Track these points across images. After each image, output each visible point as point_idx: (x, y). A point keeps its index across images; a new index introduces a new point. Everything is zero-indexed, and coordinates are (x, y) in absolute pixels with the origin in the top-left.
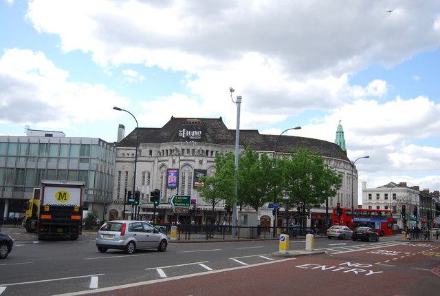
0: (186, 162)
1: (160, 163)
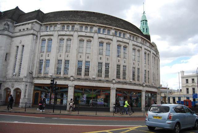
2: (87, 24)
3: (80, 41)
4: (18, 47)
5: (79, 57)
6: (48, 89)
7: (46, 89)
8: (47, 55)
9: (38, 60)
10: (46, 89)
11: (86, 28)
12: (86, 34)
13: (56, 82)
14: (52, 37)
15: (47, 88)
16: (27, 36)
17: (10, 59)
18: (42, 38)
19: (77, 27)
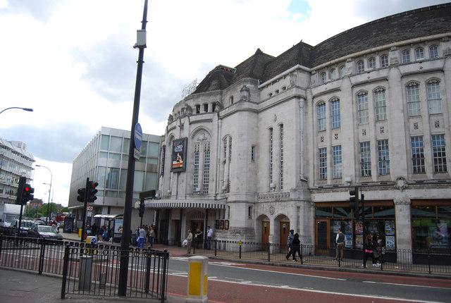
0: (199, 125)
2: (421, 42)
3: (408, 86)
4: (271, 129)
5: (412, 127)
6: (345, 213)
7: (342, 214)
8: (334, 136)
9: (316, 151)
10: (342, 214)
11: (420, 51)
12: (421, 68)
13: (363, 196)
14: (338, 94)
15: (342, 211)
16: (276, 107)
17: (261, 157)
18: (316, 100)
19: (394, 55)
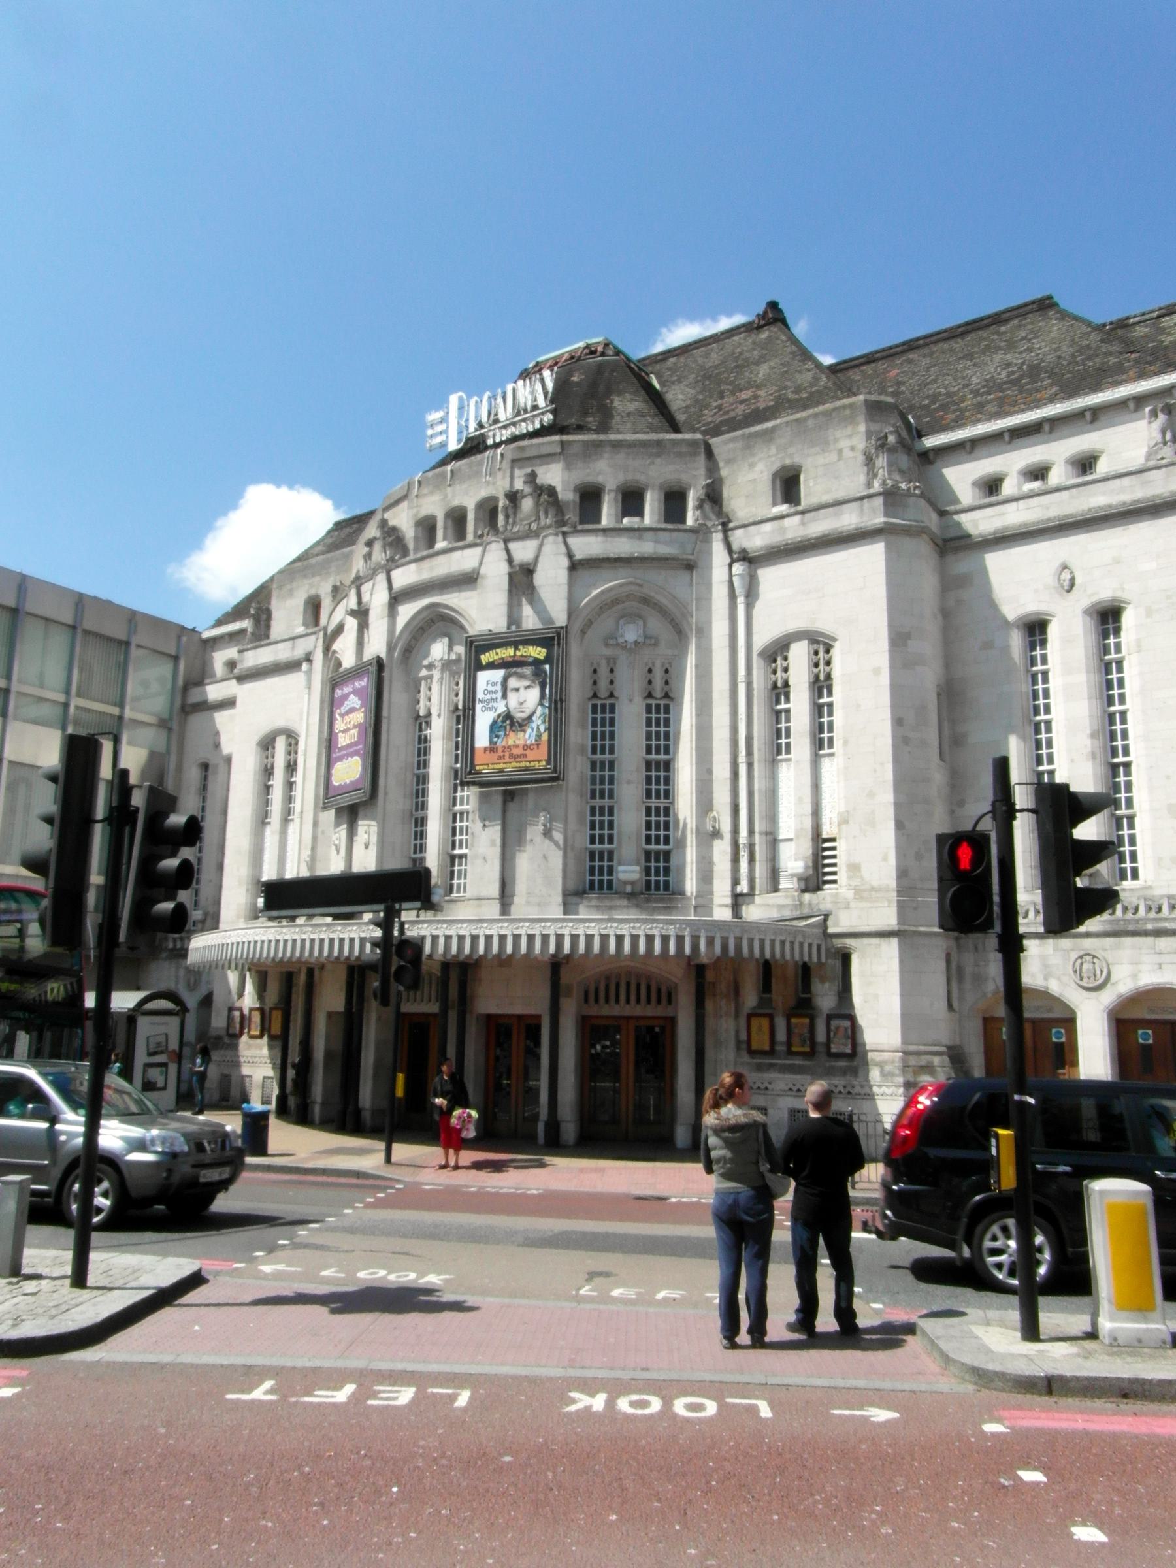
1: (407, 611)
